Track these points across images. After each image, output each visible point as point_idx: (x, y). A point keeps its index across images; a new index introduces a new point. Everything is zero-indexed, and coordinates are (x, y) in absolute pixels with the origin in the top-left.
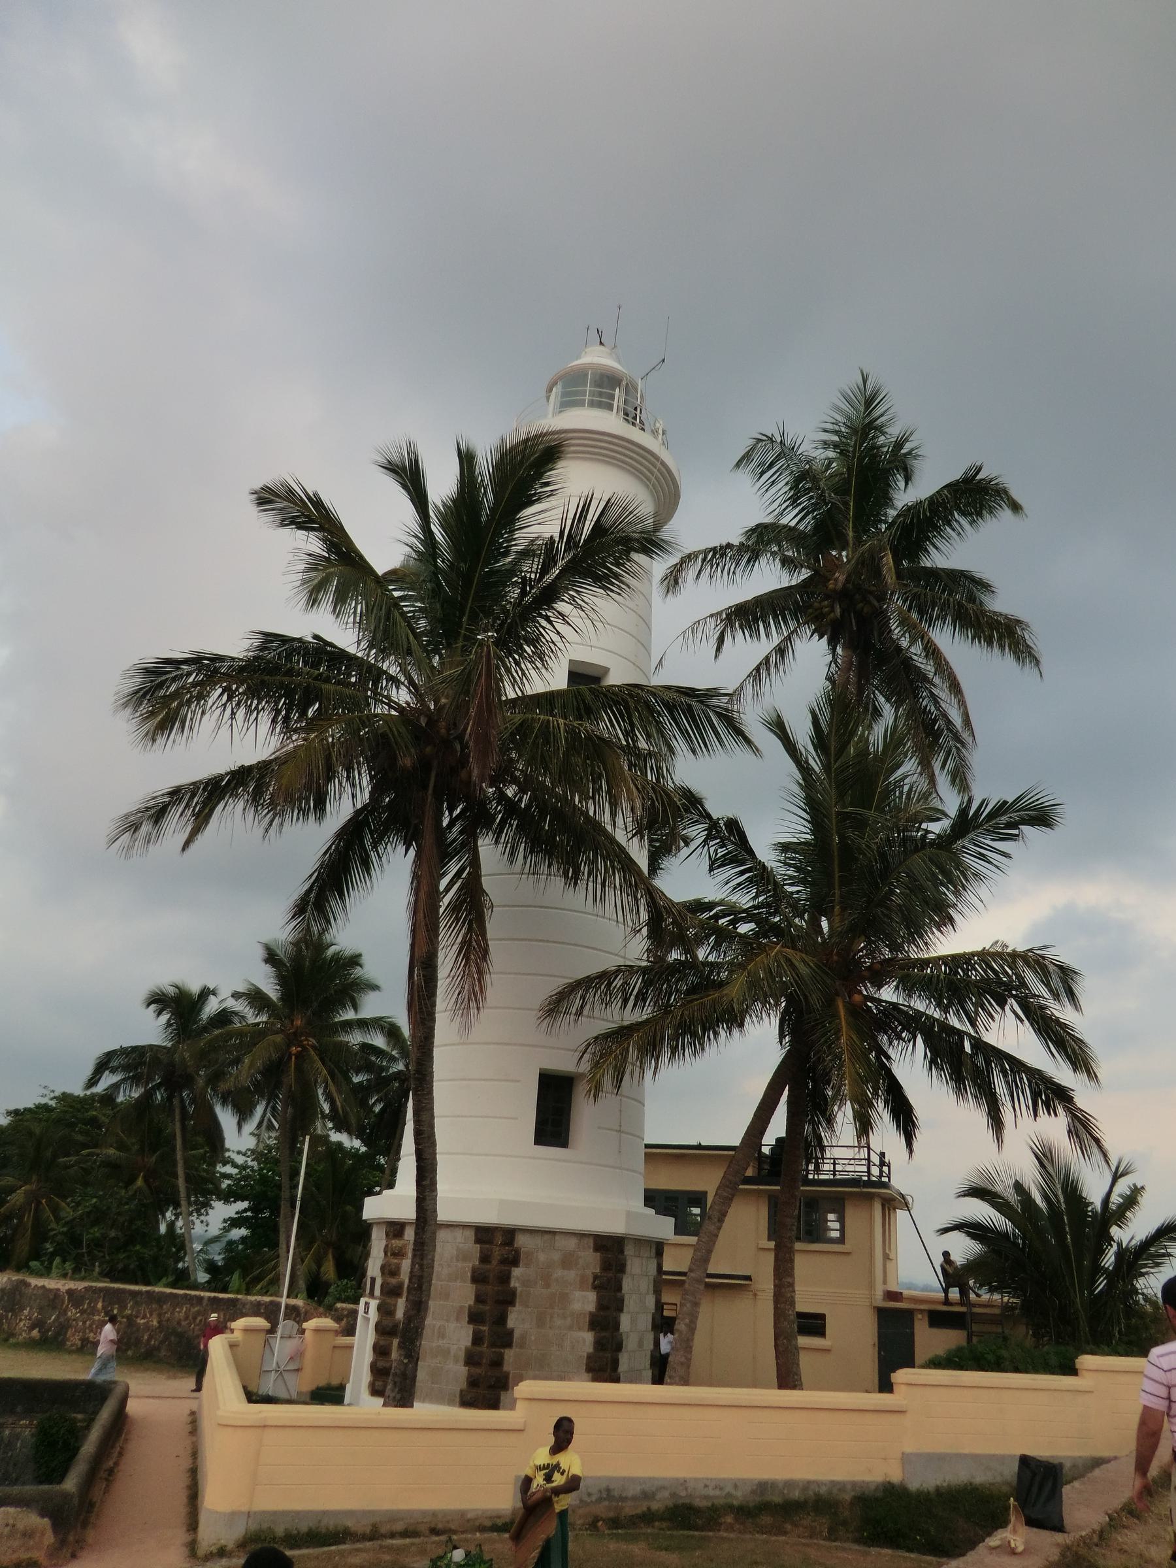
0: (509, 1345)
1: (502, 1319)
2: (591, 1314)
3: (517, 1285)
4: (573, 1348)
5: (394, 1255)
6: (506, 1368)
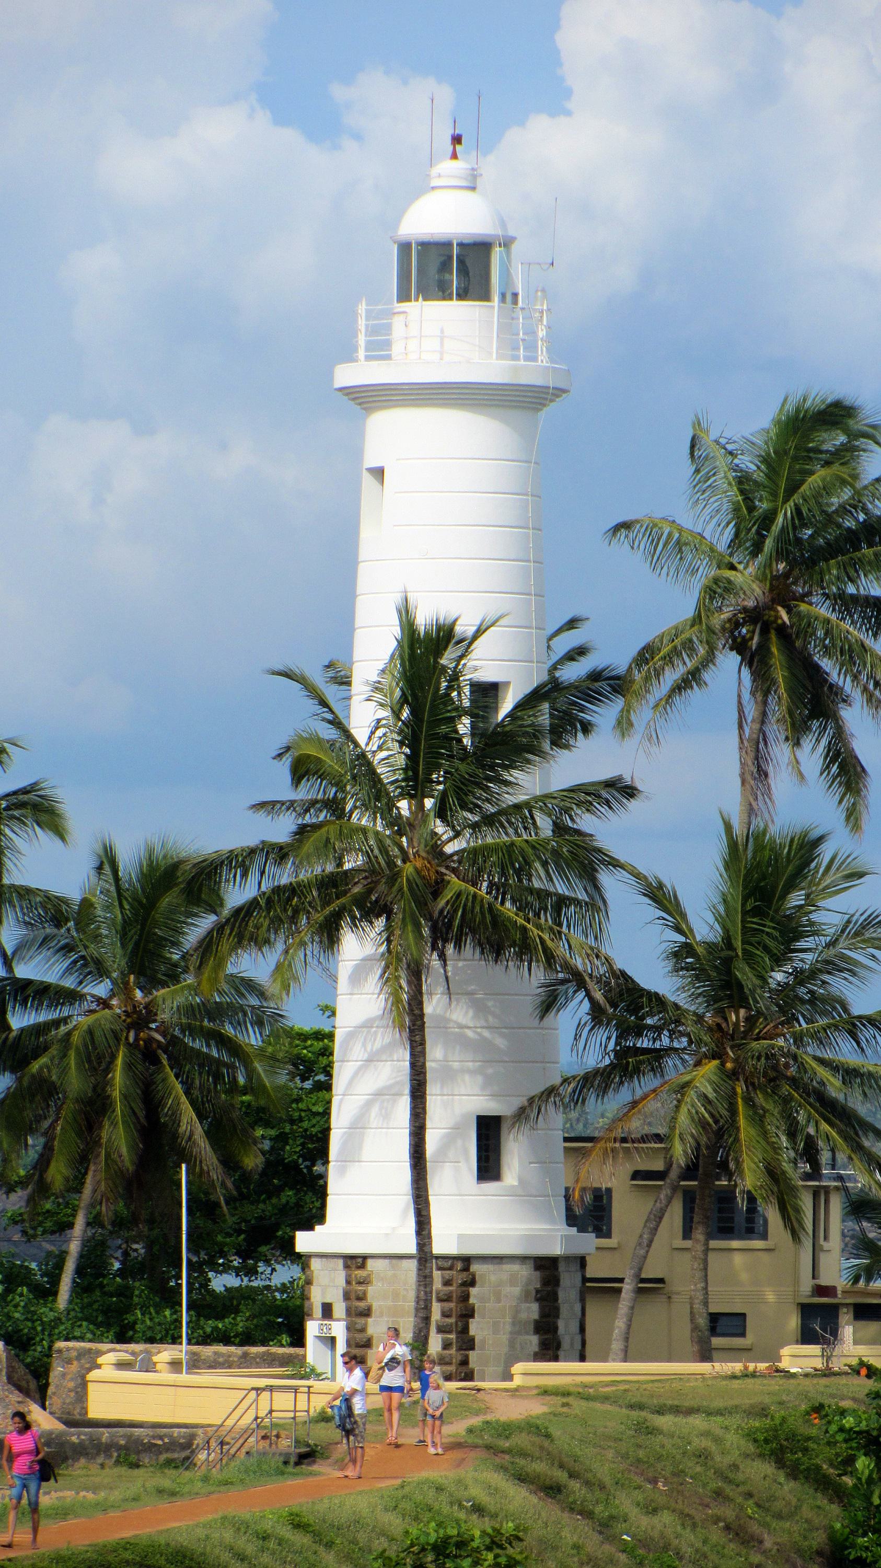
0: (473, 1349)
1: (465, 1329)
2: (536, 1322)
3: (475, 1302)
4: (522, 1348)
5: (358, 1346)
6: (471, 1365)
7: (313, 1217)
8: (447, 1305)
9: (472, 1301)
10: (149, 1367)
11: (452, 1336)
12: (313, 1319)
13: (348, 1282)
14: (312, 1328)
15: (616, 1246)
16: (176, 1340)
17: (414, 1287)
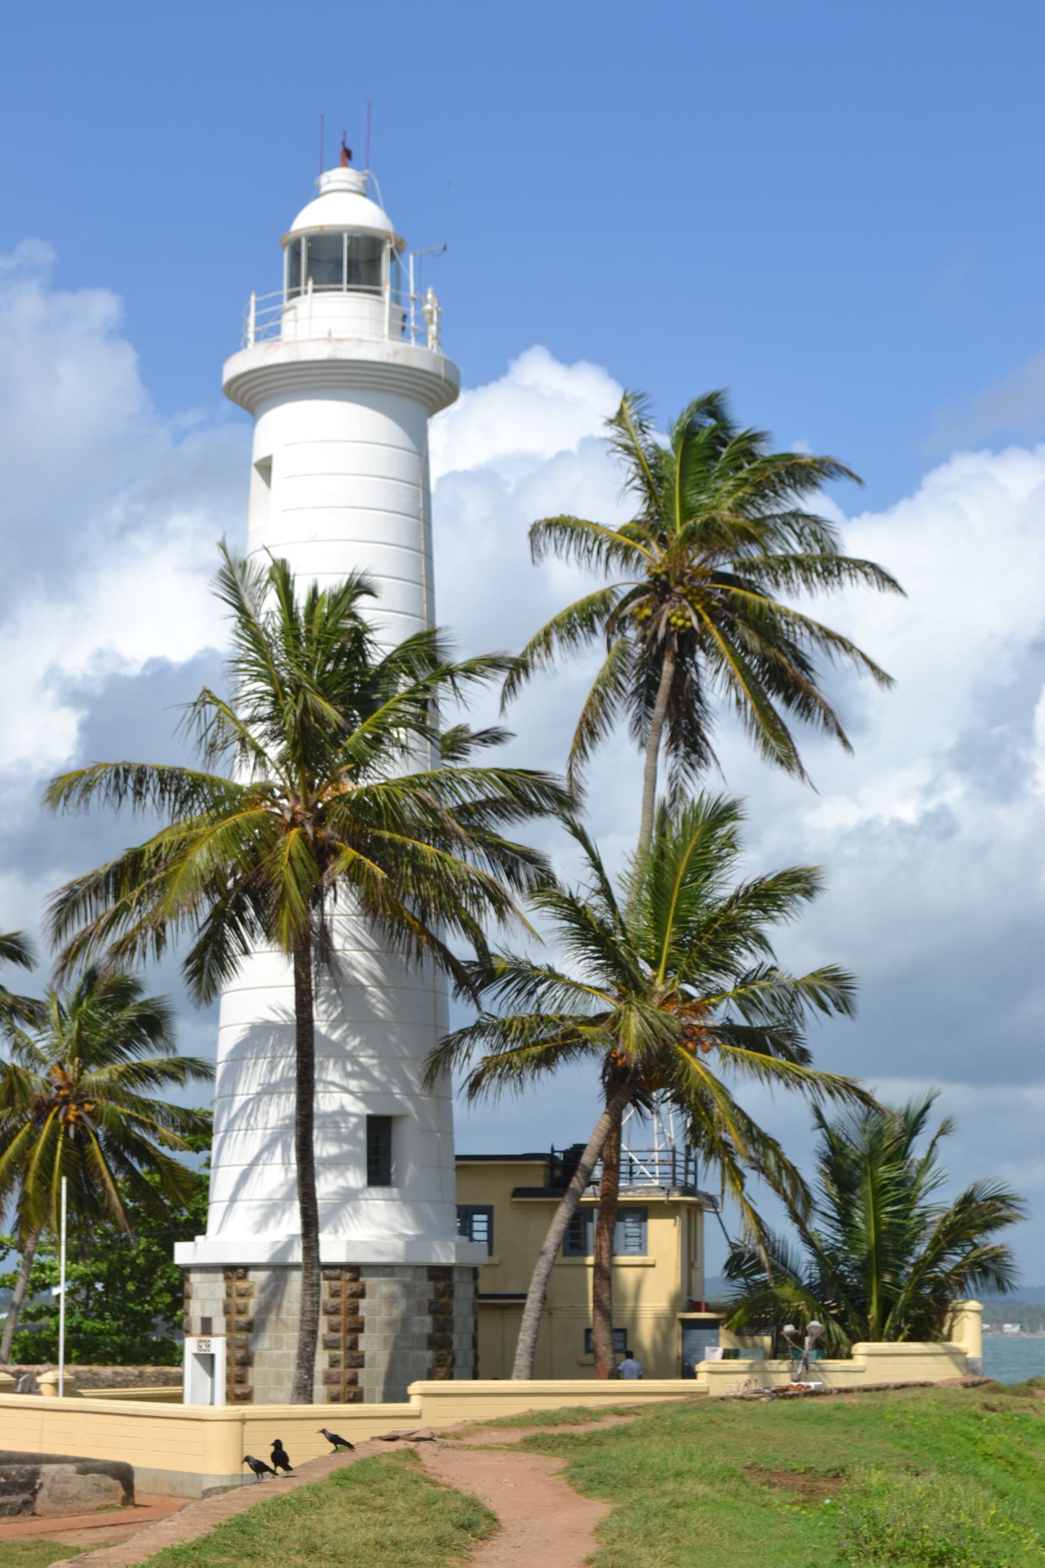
0: (362, 1366)
1: (354, 1346)
6: (360, 1384)
7: (195, 1227)
8: (335, 1319)
9: (361, 1313)
10: (31, 1388)
11: (340, 1353)
12: (191, 1335)
13: (229, 1295)
14: (191, 1345)
15: (497, 1262)
16: (54, 1360)
17: (299, 1299)
